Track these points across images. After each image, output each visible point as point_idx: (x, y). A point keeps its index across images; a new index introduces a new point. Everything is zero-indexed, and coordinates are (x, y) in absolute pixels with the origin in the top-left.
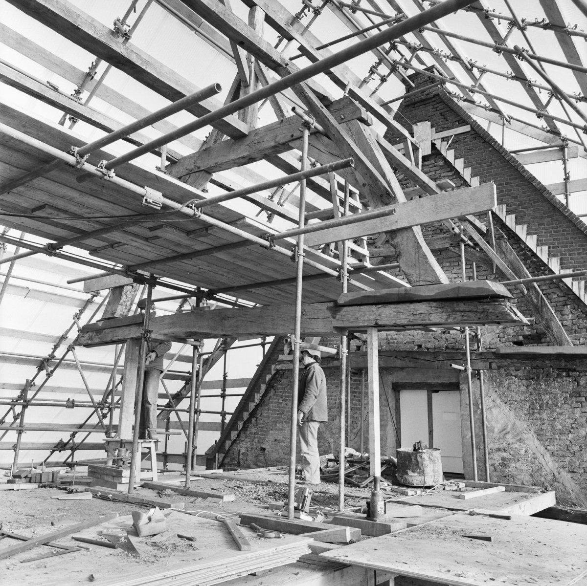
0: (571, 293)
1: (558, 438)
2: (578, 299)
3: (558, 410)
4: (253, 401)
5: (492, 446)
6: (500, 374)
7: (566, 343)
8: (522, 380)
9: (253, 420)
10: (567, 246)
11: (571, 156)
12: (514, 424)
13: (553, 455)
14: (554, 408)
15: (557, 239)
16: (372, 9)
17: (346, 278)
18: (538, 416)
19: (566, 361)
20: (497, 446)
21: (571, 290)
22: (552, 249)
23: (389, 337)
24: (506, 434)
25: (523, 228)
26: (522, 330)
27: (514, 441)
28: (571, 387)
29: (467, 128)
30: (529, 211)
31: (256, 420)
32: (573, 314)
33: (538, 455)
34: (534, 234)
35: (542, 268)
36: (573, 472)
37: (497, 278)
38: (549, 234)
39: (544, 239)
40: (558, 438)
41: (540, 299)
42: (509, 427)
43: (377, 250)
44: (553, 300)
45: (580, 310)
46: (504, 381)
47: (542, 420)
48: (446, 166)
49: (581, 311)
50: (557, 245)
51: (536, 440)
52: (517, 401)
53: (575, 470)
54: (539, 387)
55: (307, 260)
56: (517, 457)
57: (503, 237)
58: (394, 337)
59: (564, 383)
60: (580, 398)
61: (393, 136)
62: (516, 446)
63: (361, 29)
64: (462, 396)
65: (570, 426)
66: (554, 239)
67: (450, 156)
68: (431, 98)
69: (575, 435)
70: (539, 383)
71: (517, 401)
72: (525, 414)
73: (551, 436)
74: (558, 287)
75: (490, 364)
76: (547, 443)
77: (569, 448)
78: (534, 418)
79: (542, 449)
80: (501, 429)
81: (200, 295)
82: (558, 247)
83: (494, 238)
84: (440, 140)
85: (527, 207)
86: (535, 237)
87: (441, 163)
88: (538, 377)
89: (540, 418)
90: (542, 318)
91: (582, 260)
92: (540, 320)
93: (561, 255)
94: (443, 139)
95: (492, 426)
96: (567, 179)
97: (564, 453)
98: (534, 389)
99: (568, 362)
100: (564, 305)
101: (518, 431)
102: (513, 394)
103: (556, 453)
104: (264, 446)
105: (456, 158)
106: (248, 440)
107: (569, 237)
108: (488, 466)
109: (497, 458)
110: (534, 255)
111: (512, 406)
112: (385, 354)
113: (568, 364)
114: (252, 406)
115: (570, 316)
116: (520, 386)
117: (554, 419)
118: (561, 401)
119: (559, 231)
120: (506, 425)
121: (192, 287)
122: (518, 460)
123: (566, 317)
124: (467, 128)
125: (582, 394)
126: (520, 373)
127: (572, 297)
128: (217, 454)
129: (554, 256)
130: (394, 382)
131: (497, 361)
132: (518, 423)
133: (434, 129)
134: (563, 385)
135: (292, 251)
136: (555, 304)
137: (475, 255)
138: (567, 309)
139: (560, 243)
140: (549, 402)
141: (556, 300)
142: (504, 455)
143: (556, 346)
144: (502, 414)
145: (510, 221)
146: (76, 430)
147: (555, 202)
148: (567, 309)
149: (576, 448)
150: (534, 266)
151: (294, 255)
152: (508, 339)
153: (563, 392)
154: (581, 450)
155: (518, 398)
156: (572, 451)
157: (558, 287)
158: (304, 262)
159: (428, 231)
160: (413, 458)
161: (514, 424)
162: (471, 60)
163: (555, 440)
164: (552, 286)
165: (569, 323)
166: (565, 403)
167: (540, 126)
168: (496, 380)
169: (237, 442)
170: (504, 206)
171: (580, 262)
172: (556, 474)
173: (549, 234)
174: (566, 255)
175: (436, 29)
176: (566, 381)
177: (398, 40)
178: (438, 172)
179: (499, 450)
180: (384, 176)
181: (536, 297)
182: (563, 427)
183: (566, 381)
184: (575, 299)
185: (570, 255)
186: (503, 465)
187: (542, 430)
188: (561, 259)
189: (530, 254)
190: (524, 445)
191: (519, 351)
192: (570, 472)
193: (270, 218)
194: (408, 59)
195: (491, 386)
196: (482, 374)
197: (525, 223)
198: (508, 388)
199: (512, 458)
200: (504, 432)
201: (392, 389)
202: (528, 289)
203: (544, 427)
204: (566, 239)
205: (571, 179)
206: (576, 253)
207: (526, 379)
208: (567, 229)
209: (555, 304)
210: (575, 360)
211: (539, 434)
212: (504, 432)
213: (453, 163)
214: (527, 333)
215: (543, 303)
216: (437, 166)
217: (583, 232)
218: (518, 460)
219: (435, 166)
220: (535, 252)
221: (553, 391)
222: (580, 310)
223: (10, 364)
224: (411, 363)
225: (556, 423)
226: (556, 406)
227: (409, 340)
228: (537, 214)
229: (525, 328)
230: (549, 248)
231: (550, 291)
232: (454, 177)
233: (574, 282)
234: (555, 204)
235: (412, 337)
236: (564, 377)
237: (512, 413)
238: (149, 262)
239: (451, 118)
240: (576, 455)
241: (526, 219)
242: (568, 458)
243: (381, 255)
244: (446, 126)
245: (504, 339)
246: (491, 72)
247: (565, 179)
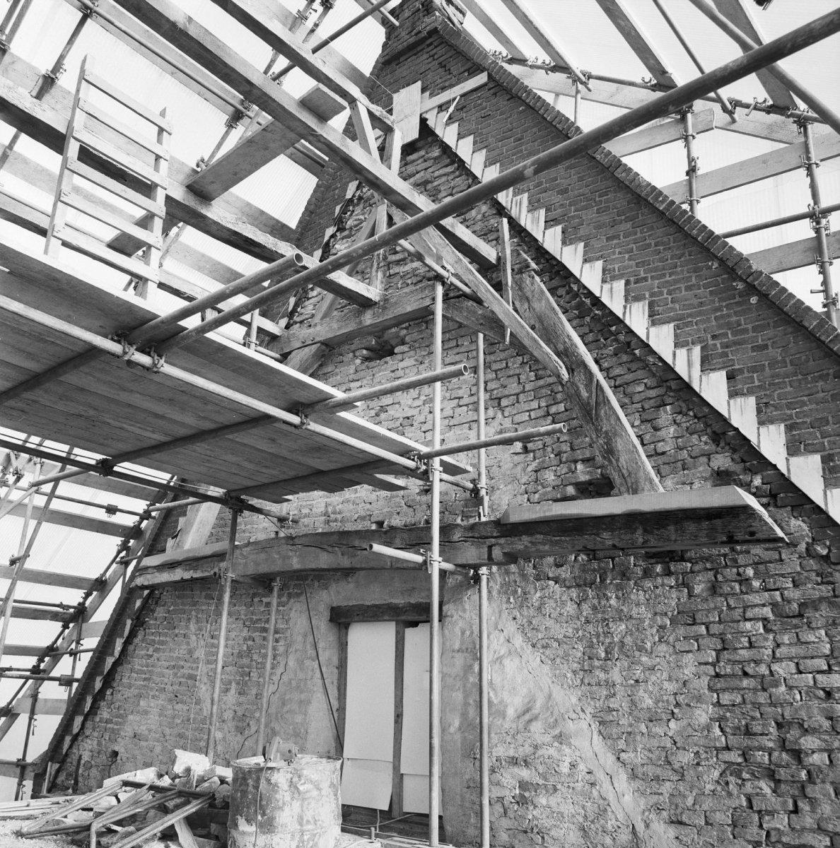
0: (672, 376)
1: (645, 730)
2: (687, 387)
3: (644, 659)
4: (112, 654)
5: (501, 751)
6: (524, 576)
7: (647, 486)
8: (569, 588)
9: (109, 692)
10: (664, 275)
11: (701, 128)
12: (550, 696)
13: (633, 776)
14: (637, 653)
15: (643, 262)
18: (602, 676)
19: (645, 531)
20: (511, 753)
21: (672, 370)
22: (632, 285)
23: (330, 509)
24: (530, 721)
25: (576, 249)
26: (573, 472)
27: (547, 738)
28: (673, 599)
29: (482, 78)
30: (591, 215)
31: (112, 694)
32: (678, 425)
33: (600, 776)
34: (598, 259)
35: (614, 328)
36: (681, 823)
37: (527, 363)
38: (627, 256)
39: (616, 266)
40: (645, 730)
41: (594, 391)
42: (538, 704)
43: (311, 330)
44: (637, 398)
45: (691, 413)
46: (532, 591)
47: (610, 685)
48: (445, 156)
49: (695, 416)
50: (643, 275)
51: (595, 736)
52: (556, 640)
53: (684, 818)
54: (603, 602)
56: (552, 781)
57: (528, 266)
58: (338, 508)
59: (658, 591)
60: (695, 628)
62: (552, 751)
64: (446, 631)
65: (672, 699)
66: (637, 265)
67: (449, 135)
68: (425, 39)
69: (685, 722)
70: (605, 595)
71: (556, 640)
72: (574, 672)
73: (631, 725)
74: (646, 366)
75: (490, 548)
76: (621, 744)
77: (671, 758)
78: (593, 682)
79: (609, 760)
80: (521, 709)
82: (645, 279)
83: (509, 271)
84: (436, 111)
85: (585, 208)
86: (599, 265)
87: (436, 152)
88: (603, 580)
89: (607, 681)
90: (598, 431)
91: (696, 301)
92: (594, 436)
93: (651, 296)
95: (501, 702)
96: (692, 171)
97: (658, 771)
98: (594, 608)
99: (652, 533)
100: (660, 406)
101: (556, 713)
102: (550, 623)
103: (640, 771)
104: (116, 749)
105: (460, 136)
106: (96, 734)
107: (669, 254)
108: (486, 802)
109: (510, 779)
110: (597, 302)
111: (548, 652)
112: (303, 541)
113: (650, 537)
114: (110, 661)
115: (672, 429)
116: (564, 603)
117: (637, 681)
118: (651, 636)
119: (649, 245)
120: (532, 700)
122: (555, 790)
123: (662, 433)
124: (482, 78)
125: (699, 616)
126: (565, 573)
127: (673, 384)
128: (50, 764)
129: (638, 299)
130: (334, 605)
131: (502, 541)
132: (558, 694)
133: (427, 94)
134: (657, 596)
136: (639, 405)
137: (475, 312)
138: (666, 416)
139: (650, 271)
140: (625, 640)
141: (643, 396)
142: (525, 774)
143: (626, 495)
144: (526, 671)
145: (551, 240)
147: (639, 185)
148: (666, 416)
149: (686, 758)
150: (599, 327)
152: (546, 493)
153: (656, 614)
154: (698, 764)
155: (559, 631)
156: (676, 766)
157: (646, 366)
159: (408, 285)
160: (250, 782)
161: (550, 696)
163: (638, 738)
164: (634, 366)
165: (667, 447)
166: (660, 641)
167: (639, 81)
168: (516, 592)
169: (80, 738)
170: (542, 212)
171: (691, 306)
172: (640, 827)
173: (627, 256)
174: (661, 293)
176: (663, 585)
178: (430, 170)
179: (514, 761)
181: (586, 386)
182: (657, 702)
183: (663, 585)
184: (680, 390)
185: (669, 293)
186: (522, 801)
187: (611, 710)
188: (651, 305)
189: (588, 301)
190: (567, 750)
191: (548, 514)
192: (672, 822)
195: (505, 606)
196: (484, 579)
197: (580, 239)
198: (539, 608)
199: (541, 782)
200: (527, 717)
201: (331, 620)
202: (571, 370)
203: (613, 703)
204: (661, 260)
205: (699, 173)
206: (683, 286)
207: (578, 586)
208: (665, 239)
209: (639, 405)
210: (664, 527)
211: (604, 721)
212: (527, 717)
213: (453, 147)
214: (583, 478)
215: (601, 398)
216: (429, 159)
217: (696, 239)
218: (555, 790)
219: (425, 161)
220: (598, 295)
221: (634, 613)
222: (691, 413)
224: (346, 557)
225: (641, 693)
226: (641, 649)
227: (363, 513)
228: (605, 218)
229: (580, 466)
230: (627, 283)
231: (630, 377)
232: (457, 173)
233: (678, 352)
234: (638, 191)
235: (368, 506)
236: (658, 575)
237: (546, 668)
238: (261, 486)
239: (456, 68)
240: (687, 778)
242: (668, 784)
243: (318, 339)
244: (447, 84)
245: (537, 496)
247: (688, 173)
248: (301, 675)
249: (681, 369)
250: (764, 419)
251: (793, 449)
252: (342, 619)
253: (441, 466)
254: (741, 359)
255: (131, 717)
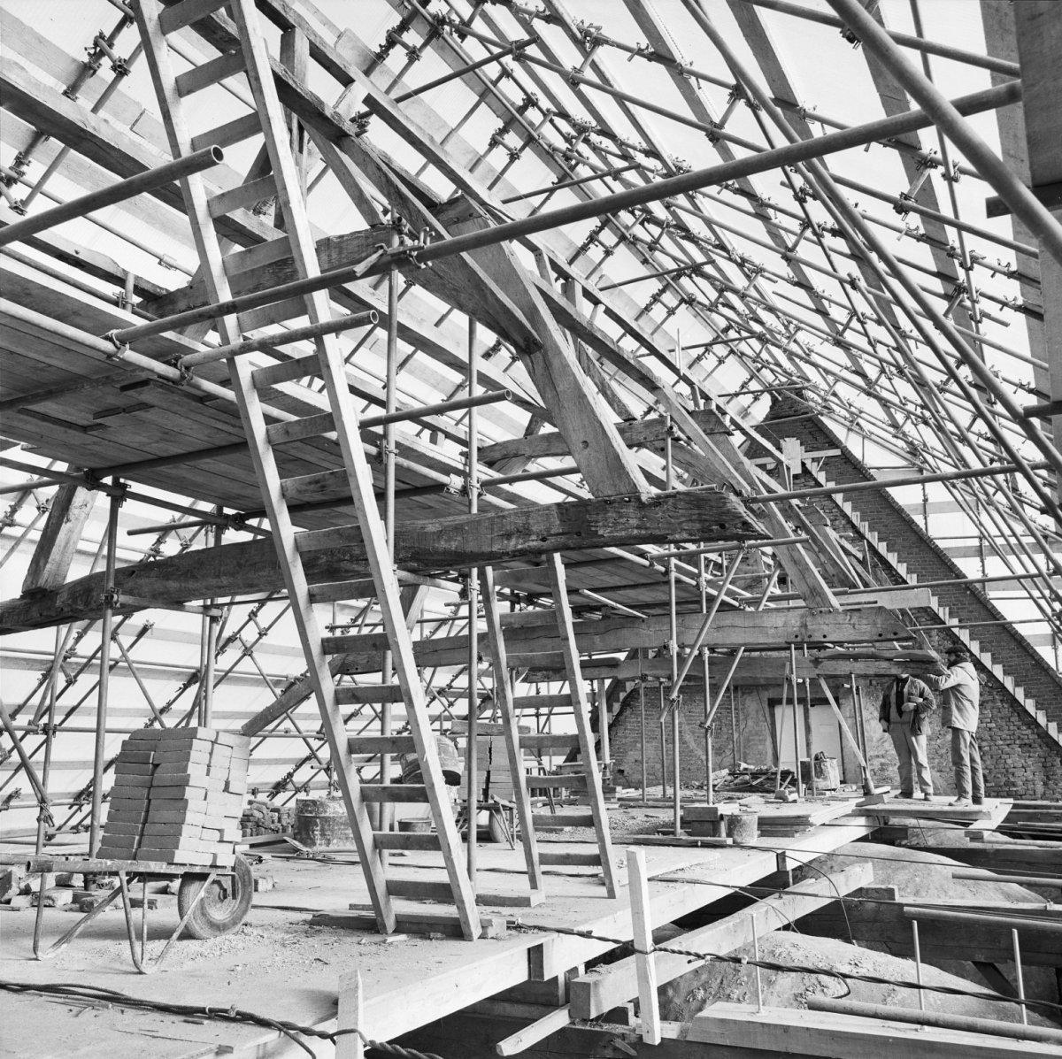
16: (495, 38)
17: (475, 492)
29: (837, 452)
30: (900, 541)
55: (402, 461)
61: (754, 451)
63: (471, 63)
81: (219, 523)
86: (905, 565)
94: (813, 460)
96: (926, 500)
121: (206, 507)
124: (837, 452)
135: (376, 446)
142: (883, 760)
145: (882, 548)
146: (362, 764)
149: (944, 751)
151: (380, 454)
158: (396, 465)
162: (582, 22)
170: (876, 533)
175: (609, 88)
177: (639, 206)
179: (878, 756)
180: (849, 571)
186: (882, 770)
193: (433, 440)
194: (466, 18)
202: (902, 615)
205: (930, 501)
223: (154, 681)
228: (906, 544)
239: (821, 439)
241: (896, 547)
246: (613, 44)
248: (757, 729)
249: (941, 615)
250: (1017, 684)
251: (982, 650)
252: (773, 703)
253: (396, 448)
254: (964, 614)
255: (630, 753)
